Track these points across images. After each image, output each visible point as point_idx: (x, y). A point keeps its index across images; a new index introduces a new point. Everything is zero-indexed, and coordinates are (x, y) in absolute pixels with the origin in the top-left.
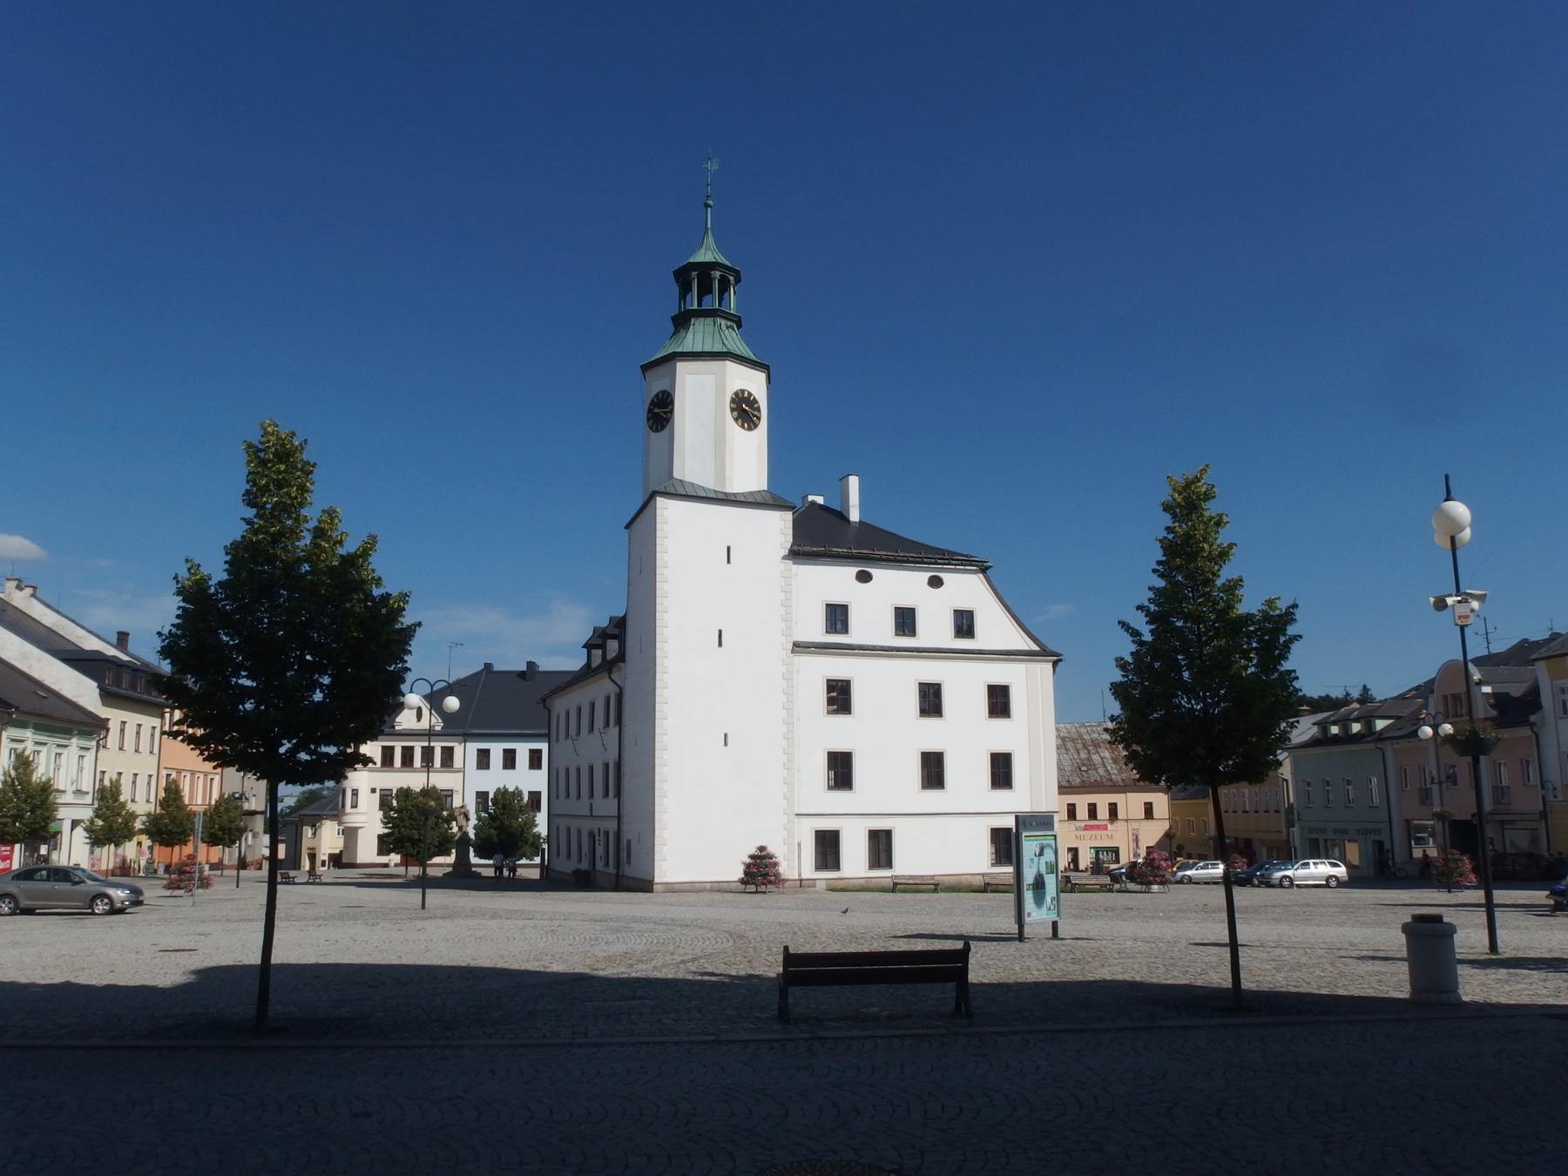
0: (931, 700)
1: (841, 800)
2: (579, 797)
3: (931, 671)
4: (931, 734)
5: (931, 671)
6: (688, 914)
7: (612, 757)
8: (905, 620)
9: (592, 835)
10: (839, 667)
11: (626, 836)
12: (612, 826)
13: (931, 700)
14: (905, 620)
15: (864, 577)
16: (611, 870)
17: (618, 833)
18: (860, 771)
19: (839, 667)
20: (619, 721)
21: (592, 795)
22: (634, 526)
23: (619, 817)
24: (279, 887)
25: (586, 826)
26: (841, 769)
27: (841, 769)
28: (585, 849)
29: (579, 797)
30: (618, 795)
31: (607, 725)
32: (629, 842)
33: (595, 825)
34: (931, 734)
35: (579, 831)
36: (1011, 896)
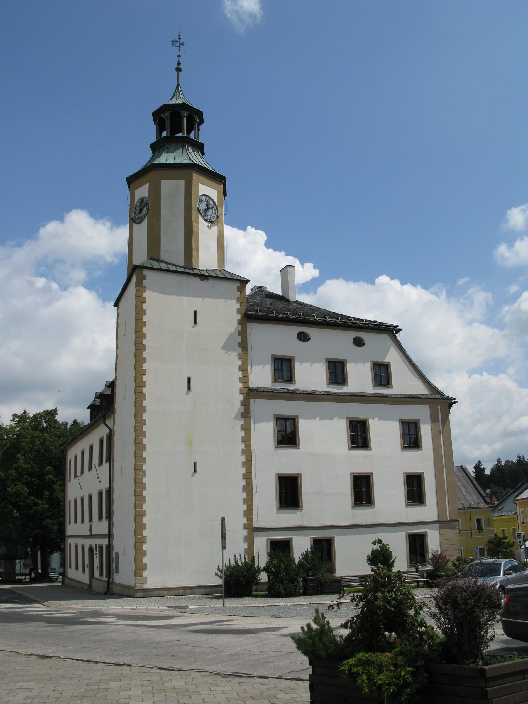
0: (359, 435)
1: (290, 518)
2: (82, 521)
3: (359, 411)
4: (360, 462)
5: (359, 411)
6: (153, 634)
7: (104, 486)
8: (337, 371)
9: (91, 550)
10: (286, 408)
11: (116, 549)
12: (105, 542)
13: (359, 435)
14: (337, 371)
15: (303, 337)
16: (105, 578)
17: (109, 547)
18: (307, 489)
19: (286, 408)
20: (110, 459)
21: (91, 520)
22: (121, 304)
23: (110, 536)
24: (438, 525)
25: (88, 543)
26: (289, 491)
27: (289, 491)
28: (87, 562)
29: (82, 521)
30: (109, 517)
31: (101, 463)
32: (117, 554)
33: (94, 542)
34: (360, 462)
35: (83, 547)
36: (89, 534)
